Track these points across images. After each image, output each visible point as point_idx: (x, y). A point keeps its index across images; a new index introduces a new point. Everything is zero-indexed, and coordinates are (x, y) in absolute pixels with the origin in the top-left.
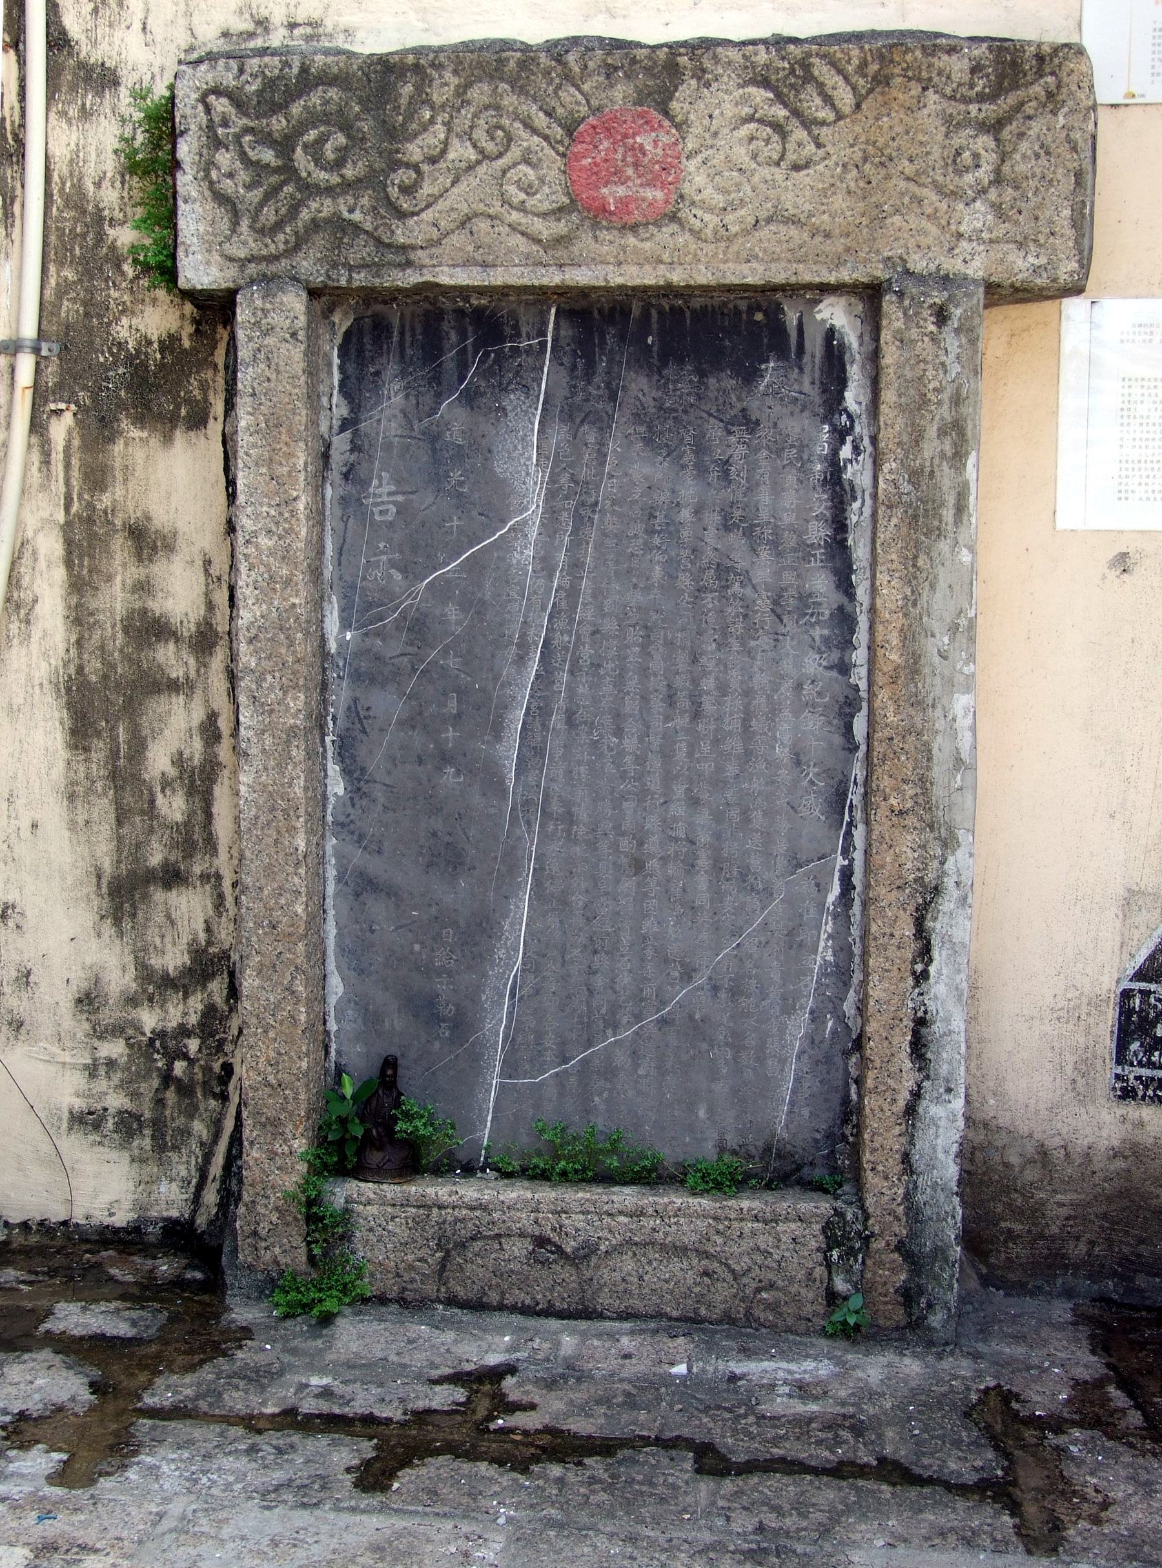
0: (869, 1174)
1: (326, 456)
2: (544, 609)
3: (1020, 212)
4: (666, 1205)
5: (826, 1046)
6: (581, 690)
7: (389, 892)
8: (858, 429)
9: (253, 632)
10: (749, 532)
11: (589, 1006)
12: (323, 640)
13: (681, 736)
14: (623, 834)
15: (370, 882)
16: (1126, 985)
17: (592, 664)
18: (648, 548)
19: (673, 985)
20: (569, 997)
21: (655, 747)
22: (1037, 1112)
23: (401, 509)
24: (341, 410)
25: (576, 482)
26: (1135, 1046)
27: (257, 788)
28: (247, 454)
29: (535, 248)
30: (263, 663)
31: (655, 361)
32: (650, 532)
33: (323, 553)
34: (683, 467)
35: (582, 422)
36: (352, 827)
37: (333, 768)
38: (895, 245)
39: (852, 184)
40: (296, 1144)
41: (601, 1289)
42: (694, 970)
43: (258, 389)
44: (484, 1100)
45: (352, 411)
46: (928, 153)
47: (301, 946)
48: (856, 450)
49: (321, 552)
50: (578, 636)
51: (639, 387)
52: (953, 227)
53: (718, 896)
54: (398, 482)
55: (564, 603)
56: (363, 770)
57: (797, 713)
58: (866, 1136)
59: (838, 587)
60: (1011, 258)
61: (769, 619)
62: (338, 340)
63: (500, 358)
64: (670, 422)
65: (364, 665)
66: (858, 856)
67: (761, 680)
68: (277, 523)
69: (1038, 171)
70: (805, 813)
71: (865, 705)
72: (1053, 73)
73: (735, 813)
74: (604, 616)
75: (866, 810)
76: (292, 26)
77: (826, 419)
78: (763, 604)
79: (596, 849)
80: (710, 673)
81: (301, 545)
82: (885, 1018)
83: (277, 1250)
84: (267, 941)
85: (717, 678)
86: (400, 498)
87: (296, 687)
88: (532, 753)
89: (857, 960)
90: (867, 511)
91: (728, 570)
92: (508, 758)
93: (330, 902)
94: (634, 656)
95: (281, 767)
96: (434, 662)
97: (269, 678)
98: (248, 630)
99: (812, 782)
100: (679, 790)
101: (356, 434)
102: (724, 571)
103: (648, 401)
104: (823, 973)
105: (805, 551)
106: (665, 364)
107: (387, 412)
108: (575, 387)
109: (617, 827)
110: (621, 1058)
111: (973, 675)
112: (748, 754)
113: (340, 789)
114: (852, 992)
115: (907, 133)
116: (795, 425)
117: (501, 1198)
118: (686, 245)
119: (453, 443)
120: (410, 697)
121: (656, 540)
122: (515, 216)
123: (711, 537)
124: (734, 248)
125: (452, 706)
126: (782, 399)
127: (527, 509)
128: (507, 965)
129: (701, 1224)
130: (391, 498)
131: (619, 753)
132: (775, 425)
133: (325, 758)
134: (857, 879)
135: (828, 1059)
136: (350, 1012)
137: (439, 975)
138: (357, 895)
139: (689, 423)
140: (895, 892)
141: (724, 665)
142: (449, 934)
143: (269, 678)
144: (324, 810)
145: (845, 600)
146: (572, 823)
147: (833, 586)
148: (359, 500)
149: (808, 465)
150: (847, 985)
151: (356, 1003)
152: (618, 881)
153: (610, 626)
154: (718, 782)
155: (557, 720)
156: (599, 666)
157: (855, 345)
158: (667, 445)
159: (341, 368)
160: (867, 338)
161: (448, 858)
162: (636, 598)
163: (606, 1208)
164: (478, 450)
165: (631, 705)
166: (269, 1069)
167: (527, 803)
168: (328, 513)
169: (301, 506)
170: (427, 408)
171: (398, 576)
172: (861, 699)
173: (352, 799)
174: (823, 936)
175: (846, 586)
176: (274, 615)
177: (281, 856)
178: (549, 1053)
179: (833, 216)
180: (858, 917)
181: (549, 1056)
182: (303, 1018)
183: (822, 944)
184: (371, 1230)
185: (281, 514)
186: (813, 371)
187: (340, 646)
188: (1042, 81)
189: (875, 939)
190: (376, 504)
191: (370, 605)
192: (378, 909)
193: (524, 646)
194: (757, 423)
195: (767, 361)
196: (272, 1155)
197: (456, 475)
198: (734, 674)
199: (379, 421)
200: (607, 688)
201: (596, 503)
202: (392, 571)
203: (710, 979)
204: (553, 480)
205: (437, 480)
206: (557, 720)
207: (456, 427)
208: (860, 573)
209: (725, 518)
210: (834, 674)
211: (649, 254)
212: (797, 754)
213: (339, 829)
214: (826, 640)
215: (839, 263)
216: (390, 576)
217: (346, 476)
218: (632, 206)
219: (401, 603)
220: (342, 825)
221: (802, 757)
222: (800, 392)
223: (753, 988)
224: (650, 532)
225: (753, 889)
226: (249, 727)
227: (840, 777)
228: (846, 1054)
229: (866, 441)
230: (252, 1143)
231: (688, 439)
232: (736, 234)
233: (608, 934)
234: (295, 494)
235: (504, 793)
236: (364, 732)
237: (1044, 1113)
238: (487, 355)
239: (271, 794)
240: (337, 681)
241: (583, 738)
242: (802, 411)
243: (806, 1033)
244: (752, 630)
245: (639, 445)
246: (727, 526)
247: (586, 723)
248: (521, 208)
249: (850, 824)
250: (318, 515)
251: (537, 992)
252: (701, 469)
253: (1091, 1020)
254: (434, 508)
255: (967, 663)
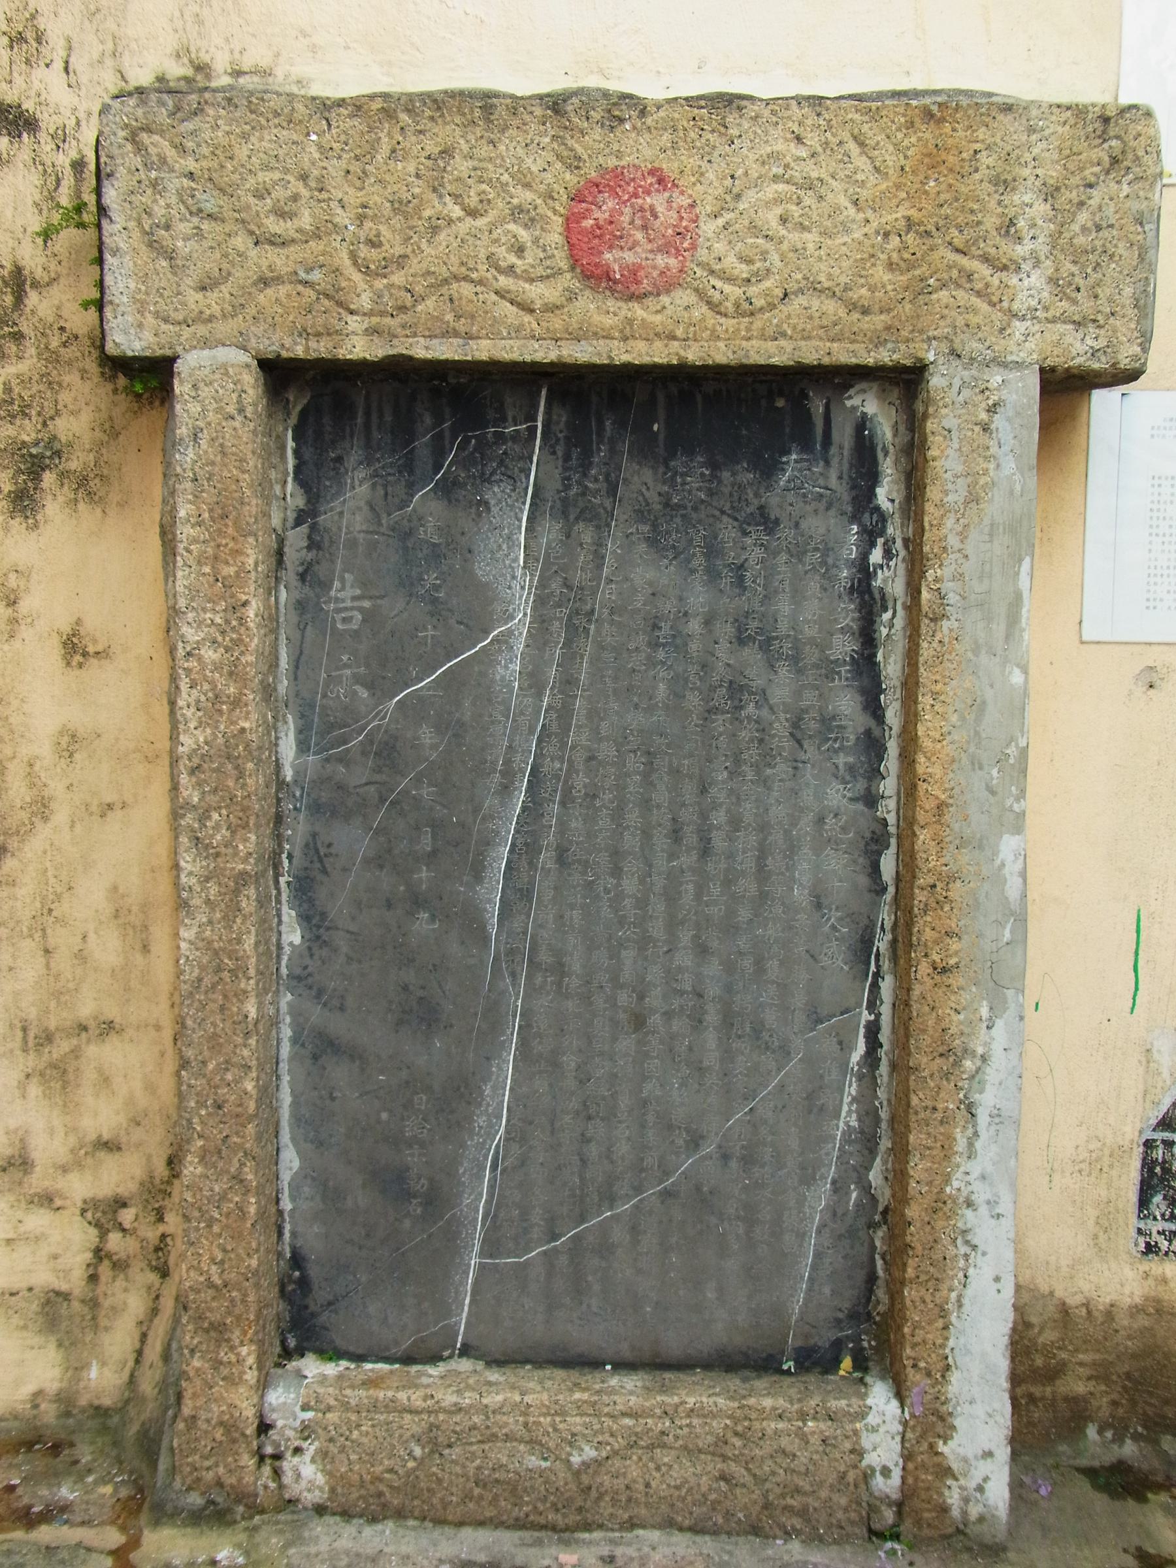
0: (910, 1371)
1: (280, 553)
2: (531, 731)
3: (1078, 290)
4: (677, 1406)
5: (849, 1220)
6: (573, 825)
7: (355, 1054)
8: (890, 530)
9: (196, 761)
10: (766, 646)
11: (582, 1179)
12: (278, 766)
13: (688, 876)
14: (622, 987)
15: (331, 1043)
16: (1149, 1135)
17: (586, 794)
18: (651, 663)
19: (677, 1154)
20: (559, 1168)
21: (658, 888)
22: (1058, 1269)
23: (369, 617)
24: (296, 499)
25: (570, 588)
26: (1158, 1199)
27: (200, 944)
28: (188, 551)
29: (527, 318)
30: (208, 798)
31: (661, 450)
32: (655, 645)
33: (277, 666)
34: (693, 571)
35: (577, 519)
36: (310, 980)
37: (289, 914)
38: (942, 323)
39: (895, 255)
40: (244, 1351)
41: (600, 1497)
42: (702, 1137)
43: (201, 473)
44: (461, 1283)
45: (309, 501)
46: (979, 223)
47: (251, 1128)
48: (888, 554)
49: (274, 665)
50: (570, 761)
51: (642, 481)
52: (1005, 304)
53: (728, 1055)
54: (364, 585)
55: (555, 725)
56: (323, 916)
57: (818, 851)
58: (906, 1330)
59: (865, 708)
60: (1069, 339)
61: (788, 744)
62: (293, 420)
63: (482, 444)
64: (678, 520)
65: (325, 796)
66: (886, 1010)
67: (778, 813)
68: (223, 633)
69: (1098, 243)
70: (825, 961)
71: (893, 841)
72: (1117, 137)
73: (747, 963)
74: (601, 740)
75: (895, 958)
76: (238, 73)
77: (855, 518)
78: (780, 727)
79: (591, 1004)
80: (721, 805)
81: (251, 658)
82: (927, 1201)
83: (221, 1470)
84: (211, 1123)
85: (728, 811)
86: (366, 604)
87: (245, 826)
88: (518, 895)
89: (884, 1125)
90: (899, 622)
91: (741, 688)
92: (490, 901)
93: (284, 1067)
94: (634, 784)
95: (228, 920)
96: (405, 792)
97: (215, 816)
98: (190, 760)
99: (834, 927)
100: (685, 937)
101: (313, 527)
102: (737, 689)
103: (652, 496)
104: (847, 1139)
105: (829, 669)
106: (672, 455)
107: (351, 504)
108: (568, 479)
109: (615, 979)
110: (619, 1235)
111: (1024, 813)
112: (763, 896)
113: (296, 938)
114: (878, 1160)
115: (957, 200)
116: (817, 525)
117: (485, 1401)
118: (703, 320)
119: (427, 542)
120: (377, 832)
121: (661, 655)
122: (504, 281)
123: (723, 651)
124: (758, 324)
125: (426, 843)
126: (804, 496)
127: (513, 618)
128: (488, 1134)
129: (717, 1425)
130: (356, 604)
131: (616, 895)
132: (797, 525)
133: (279, 902)
134: (884, 1036)
135: (852, 1233)
136: (306, 1189)
137: (410, 1146)
138: (315, 1057)
139: (700, 521)
140: (938, 1061)
141: (737, 797)
142: (422, 1101)
143: (215, 816)
144: (279, 962)
145: (872, 723)
146: (563, 974)
147: (859, 707)
148: (318, 603)
149: (834, 571)
150: (872, 1151)
151: (314, 1179)
152: (614, 1039)
153: (607, 751)
154: (730, 928)
155: (546, 858)
156: (595, 796)
157: (889, 435)
158: (674, 547)
159: (297, 453)
160: (902, 428)
161: (421, 1014)
162: (636, 720)
163: (606, 1410)
164: (451, 551)
165: (631, 841)
166: (214, 1268)
167: (511, 952)
168: (281, 620)
169: (251, 613)
170: (397, 501)
171: (364, 693)
172: (889, 835)
173: (310, 948)
174: (847, 1099)
175: (875, 710)
176: (220, 741)
177: (228, 1024)
178: (536, 1229)
179: (872, 289)
180: (885, 1079)
181: (536, 1233)
182: (252, 1210)
183: (845, 1108)
184: (331, 1440)
185: (227, 622)
186: (840, 463)
187: (297, 773)
188: (1106, 146)
189: (916, 1113)
190: (338, 611)
191: (332, 727)
192: (340, 1073)
193: (509, 774)
194: (777, 522)
195: (789, 453)
196: (217, 1364)
197: (431, 578)
198: (748, 806)
199: (341, 513)
200: (604, 822)
201: (593, 611)
202: (357, 687)
203: (720, 1147)
204: (543, 584)
205: (408, 584)
206: (546, 858)
207: (431, 522)
208: (890, 692)
209: (739, 630)
210: (860, 806)
211: (659, 329)
212: (818, 897)
213: (295, 983)
214: (851, 769)
215: (879, 343)
216: (355, 693)
217: (302, 577)
218: (641, 273)
219: (368, 724)
220: (299, 979)
221: (823, 900)
222: (827, 488)
223: (767, 1158)
224: (655, 645)
225: (767, 1048)
226: (190, 874)
227: (866, 921)
228: (872, 1225)
229: (899, 544)
230: (192, 1351)
231: (698, 540)
232: (761, 309)
233: (604, 1098)
234: (244, 598)
235: (486, 939)
236: (325, 871)
237: (1065, 1269)
238: (466, 441)
239: (216, 953)
240: (294, 814)
241: (576, 878)
242: (827, 509)
243: (827, 1205)
244: (768, 757)
245: (643, 547)
246: (741, 640)
247: (579, 861)
248: (510, 270)
249: (877, 975)
250: (271, 622)
251: (523, 1164)
252: (713, 575)
253: (1114, 1173)
254: (405, 615)
255: (1018, 800)
